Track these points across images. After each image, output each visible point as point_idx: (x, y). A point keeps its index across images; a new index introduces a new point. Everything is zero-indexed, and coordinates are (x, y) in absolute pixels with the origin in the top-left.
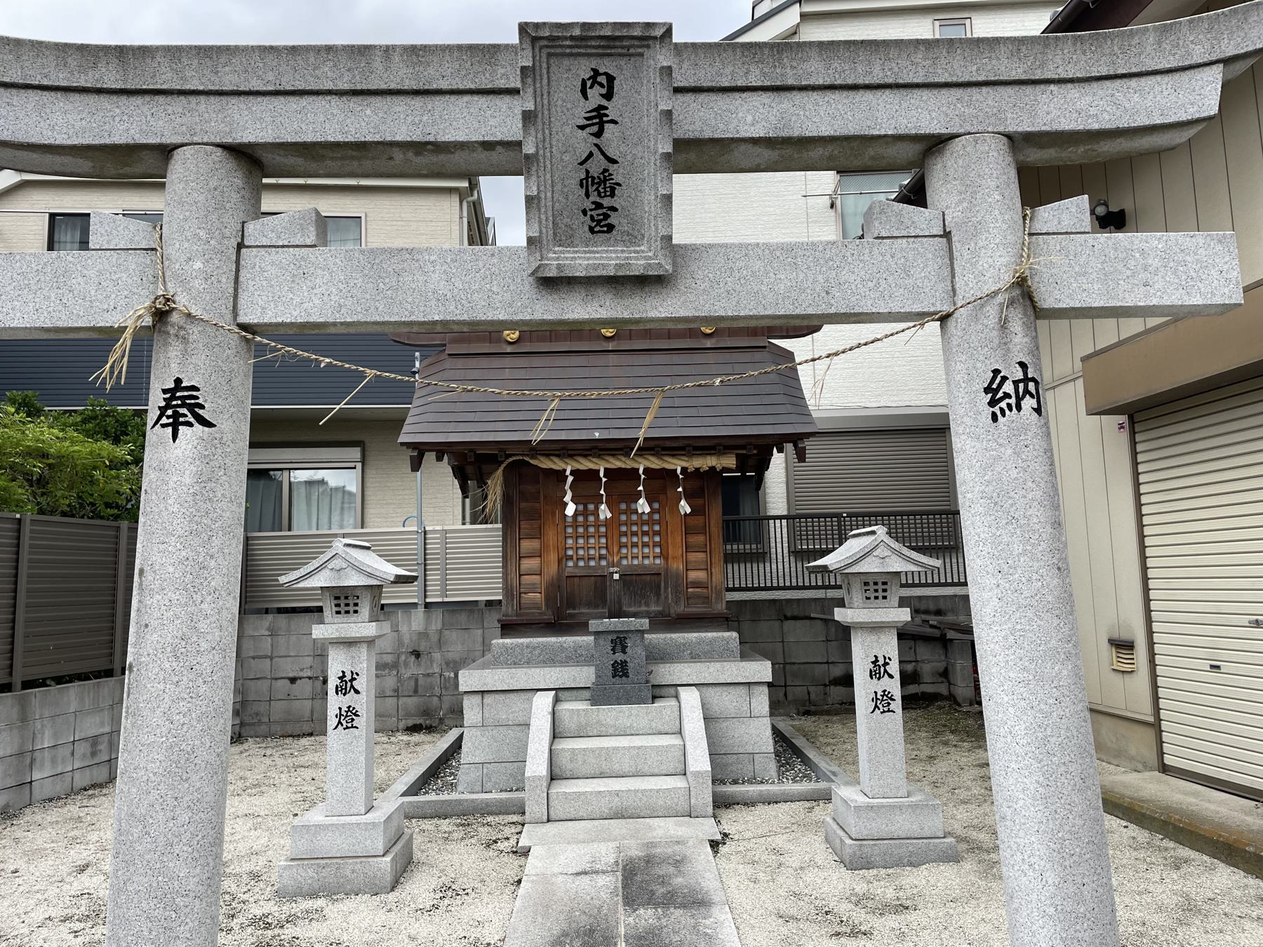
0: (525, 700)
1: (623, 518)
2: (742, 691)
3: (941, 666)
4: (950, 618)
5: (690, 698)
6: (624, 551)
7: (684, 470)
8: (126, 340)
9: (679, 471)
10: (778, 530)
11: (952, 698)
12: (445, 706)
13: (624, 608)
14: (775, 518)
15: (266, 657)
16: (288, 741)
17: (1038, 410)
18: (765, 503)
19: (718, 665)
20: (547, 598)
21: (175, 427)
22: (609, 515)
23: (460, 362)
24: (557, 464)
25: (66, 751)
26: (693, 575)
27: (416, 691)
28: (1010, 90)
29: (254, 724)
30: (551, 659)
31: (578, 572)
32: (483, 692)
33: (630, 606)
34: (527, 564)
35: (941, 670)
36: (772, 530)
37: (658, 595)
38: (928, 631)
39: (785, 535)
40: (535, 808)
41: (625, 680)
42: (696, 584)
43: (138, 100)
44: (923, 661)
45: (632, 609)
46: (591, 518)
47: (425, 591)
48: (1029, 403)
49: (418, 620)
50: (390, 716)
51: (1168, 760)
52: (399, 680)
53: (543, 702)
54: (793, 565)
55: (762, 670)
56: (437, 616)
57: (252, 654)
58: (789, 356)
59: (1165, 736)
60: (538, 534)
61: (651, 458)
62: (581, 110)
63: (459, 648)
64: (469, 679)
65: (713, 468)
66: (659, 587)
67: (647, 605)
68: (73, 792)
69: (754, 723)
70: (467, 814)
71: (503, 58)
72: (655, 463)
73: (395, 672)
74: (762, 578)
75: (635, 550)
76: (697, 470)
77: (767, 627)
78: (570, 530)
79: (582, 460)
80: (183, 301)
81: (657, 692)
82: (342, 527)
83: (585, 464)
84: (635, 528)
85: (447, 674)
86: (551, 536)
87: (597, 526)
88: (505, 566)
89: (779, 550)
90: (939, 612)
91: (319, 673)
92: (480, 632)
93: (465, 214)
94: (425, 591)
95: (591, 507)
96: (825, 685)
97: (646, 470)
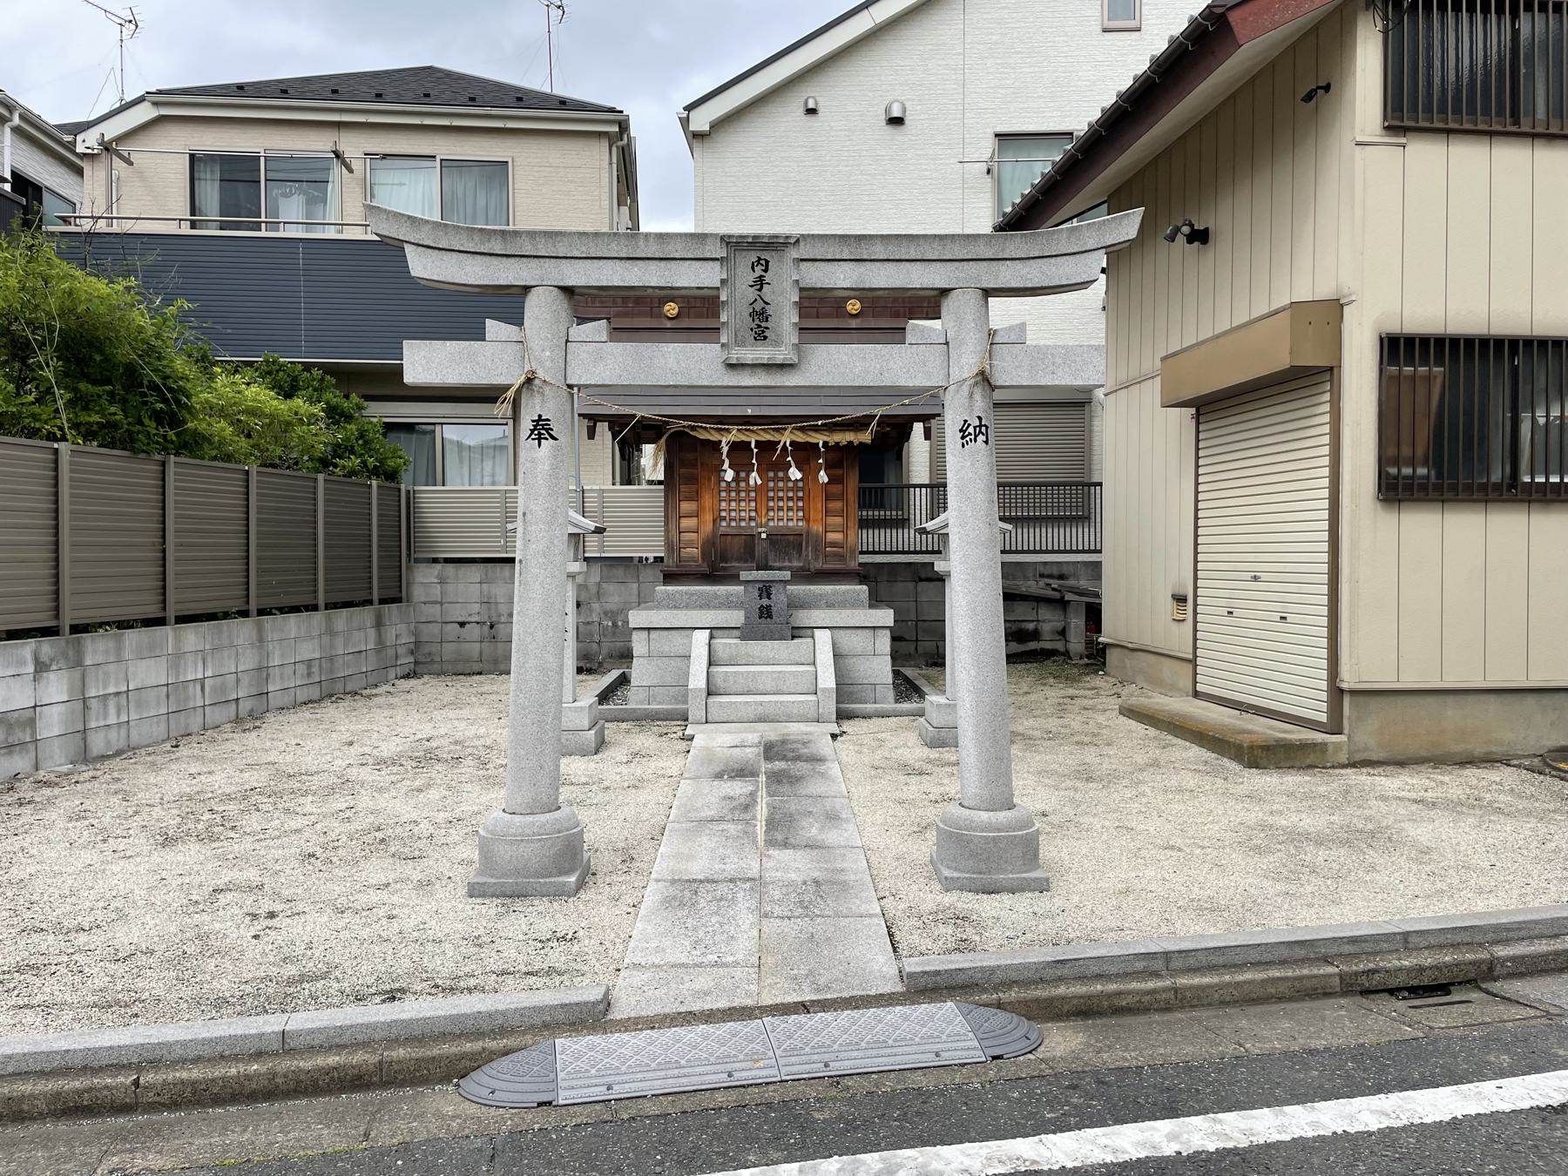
0: (685, 635)
1: (771, 484)
2: (869, 633)
3: (1060, 625)
4: (1071, 582)
5: (823, 637)
7: (825, 443)
8: (513, 389)
11: (1066, 654)
12: (604, 652)
14: (915, 486)
17: (986, 442)
19: (849, 612)
20: (703, 554)
21: (539, 440)
25: (289, 670)
26: (832, 536)
28: (985, 264)
30: (707, 604)
31: (730, 531)
34: (687, 523)
37: (800, 552)
38: (1050, 593)
40: (696, 712)
41: (769, 621)
42: (834, 544)
43: (512, 260)
48: (981, 438)
51: (1199, 688)
53: (701, 637)
55: (886, 617)
56: (596, 568)
59: (1199, 669)
60: (695, 497)
62: (751, 277)
63: (616, 599)
64: (637, 618)
68: (297, 705)
69: (877, 660)
70: (643, 719)
71: (709, 240)
77: (903, 587)
80: (541, 374)
81: (796, 633)
82: (493, 483)
86: (707, 499)
87: (748, 491)
88: (666, 524)
90: (1061, 577)
92: (635, 586)
93: (614, 160)
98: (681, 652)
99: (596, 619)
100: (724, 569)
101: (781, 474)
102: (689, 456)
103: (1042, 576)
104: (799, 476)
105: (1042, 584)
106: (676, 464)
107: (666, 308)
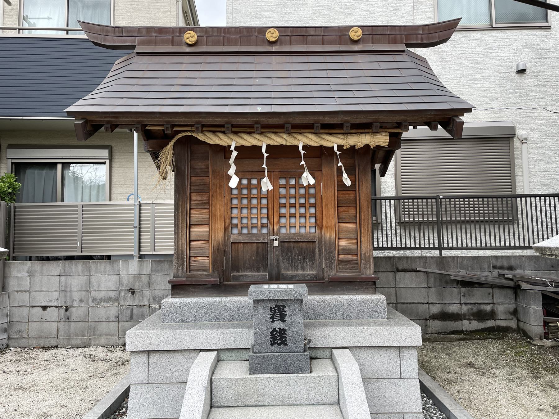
2: (394, 354)
3: (512, 307)
4: (519, 272)
5: (348, 364)
6: (283, 220)
7: (340, 147)
9: (335, 149)
10: (388, 208)
11: (525, 334)
13: (283, 272)
14: (386, 199)
15: (26, 291)
16: (38, 352)
18: (514, 148)
22: (271, 188)
23: (145, 59)
24: (222, 140)
27: (131, 318)
29: (17, 338)
30: (216, 319)
32: (149, 352)
33: (288, 270)
34: (197, 231)
35: (512, 310)
36: (383, 207)
37: (313, 260)
38: (505, 282)
39: (393, 211)
41: (283, 348)
42: (347, 251)
44: (498, 304)
45: (290, 273)
46: (255, 192)
47: (140, 246)
49: (133, 266)
50: (112, 335)
52: (120, 310)
53: (200, 369)
54: (398, 232)
57: (16, 289)
58: (423, 60)
60: (206, 205)
61: (310, 136)
65: (367, 146)
66: (314, 253)
67: (303, 269)
69: (403, 384)
72: (313, 140)
73: (116, 304)
74: (394, 241)
75: (293, 220)
76: (353, 147)
78: (235, 202)
79: (245, 136)
82: (98, 200)
83: (249, 141)
84: (293, 201)
85: (153, 306)
86: (218, 206)
87: (260, 199)
88: (176, 233)
89: (389, 221)
90: (510, 268)
91: (63, 304)
94: (140, 246)
95: (254, 182)
96: (426, 319)
97: (305, 147)
98: (181, 381)
99: (147, 303)
100: (236, 278)
101: (293, 182)
102: (200, 164)
103: (495, 267)
104: (312, 181)
105: (495, 273)
106: (187, 172)
107: (186, 35)
